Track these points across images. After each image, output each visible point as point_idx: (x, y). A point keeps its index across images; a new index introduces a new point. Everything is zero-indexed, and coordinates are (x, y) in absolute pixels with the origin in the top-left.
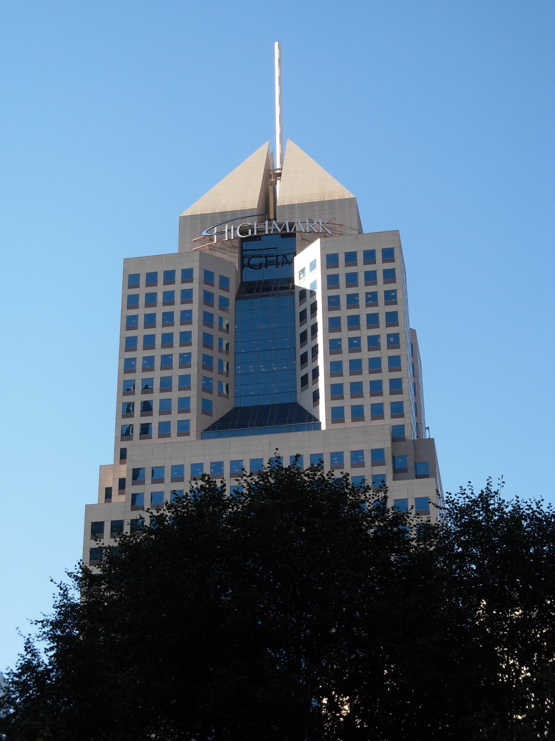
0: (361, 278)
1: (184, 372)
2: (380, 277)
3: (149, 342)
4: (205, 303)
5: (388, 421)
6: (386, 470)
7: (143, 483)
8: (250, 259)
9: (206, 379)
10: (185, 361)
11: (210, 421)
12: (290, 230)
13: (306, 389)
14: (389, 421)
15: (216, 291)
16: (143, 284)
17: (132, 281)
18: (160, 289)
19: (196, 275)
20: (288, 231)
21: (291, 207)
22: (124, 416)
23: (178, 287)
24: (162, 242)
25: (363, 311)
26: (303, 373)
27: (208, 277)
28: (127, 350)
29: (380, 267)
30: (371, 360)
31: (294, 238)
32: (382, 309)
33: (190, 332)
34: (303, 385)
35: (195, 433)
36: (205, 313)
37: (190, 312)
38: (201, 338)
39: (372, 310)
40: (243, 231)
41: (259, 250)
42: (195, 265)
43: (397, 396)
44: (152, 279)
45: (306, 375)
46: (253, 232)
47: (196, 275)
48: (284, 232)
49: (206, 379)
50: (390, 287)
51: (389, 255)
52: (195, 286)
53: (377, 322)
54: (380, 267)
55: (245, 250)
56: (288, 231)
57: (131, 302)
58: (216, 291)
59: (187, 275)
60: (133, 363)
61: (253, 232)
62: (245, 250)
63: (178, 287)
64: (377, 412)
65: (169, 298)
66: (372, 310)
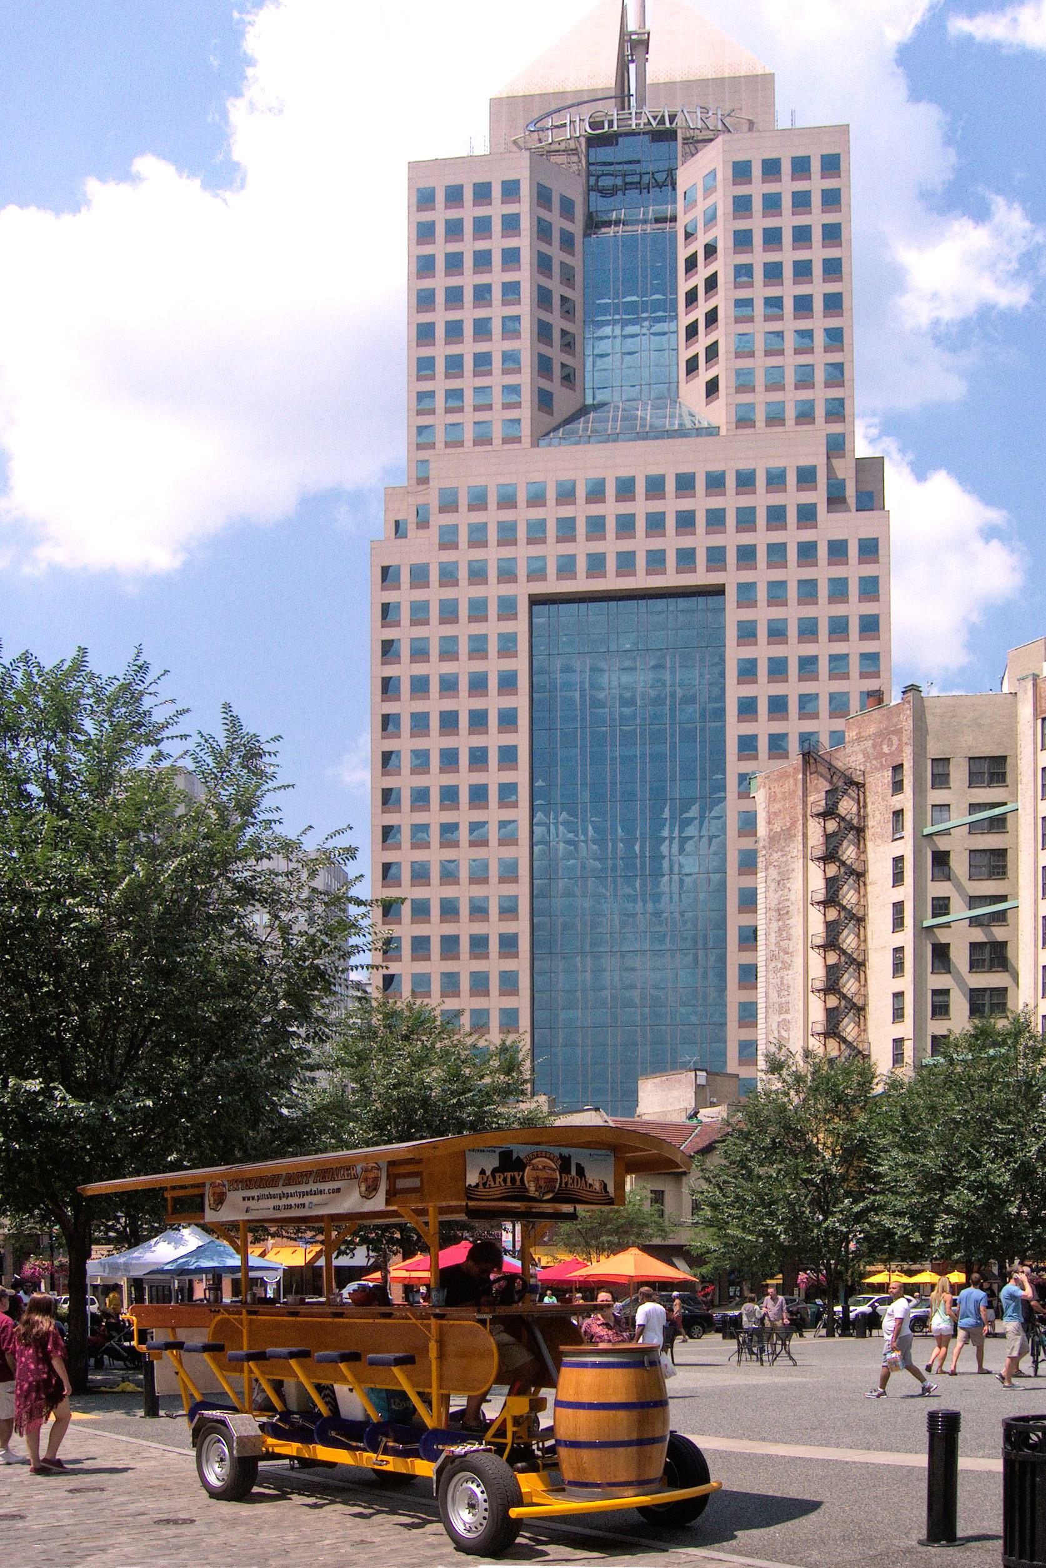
0: (787, 202)
1: (509, 345)
2: (816, 200)
3: (454, 331)
4: (539, 204)
5: (822, 429)
6: (818, 497)
7: (397, 624)
8: (598, 177)
9: (541, 255)
10: (511, 327)
11: (549, 421)
12: (671, 123)
13: (694, 378)
14: (822, 429)
15: (558, 222)
16: (442, 203)
17: (424, 199)
18: (468, 213)
19: (525, 190)
20: (668, 125)
21: (671, 85)
22: (419, 209)
23: (496, 210)
24: (462, 133)
25: (787, 221)
26: (690, 353)
27: (543, 196)
28: (419, 209)
29: (816, 185)
30: (833, 581)
31: (673, 143)
32: (818, 288)
33: (518, 215)
34: (687, 270)
35: (528, 199)
36: (540, 287)
37: (517, 318)
38: (536, 326)
39: (801, 186)
40: (594, 125)
41: (626, 163)
42: (520, 170)
43: (1000, 1504)
44: (454, 195)
45: (696, 356)
46: (611, 125)
47: (525, 190)
48: (661, 127)
49: (541, 255)
50: (833, 253)
51: (832, 165)
52: (524, 208)
53: (779, 172)
54: (816, 185)
55: (593, 164)
56: (668, 125)
57: (424, 233)
58: (558, 222)
59: (511, 190)
60: (238, 1154)
61: (611, 125)
62: (593, 164)
63: (496, 210)
64: (805, 416)
65: (482, 227)
66: (801, 186)
